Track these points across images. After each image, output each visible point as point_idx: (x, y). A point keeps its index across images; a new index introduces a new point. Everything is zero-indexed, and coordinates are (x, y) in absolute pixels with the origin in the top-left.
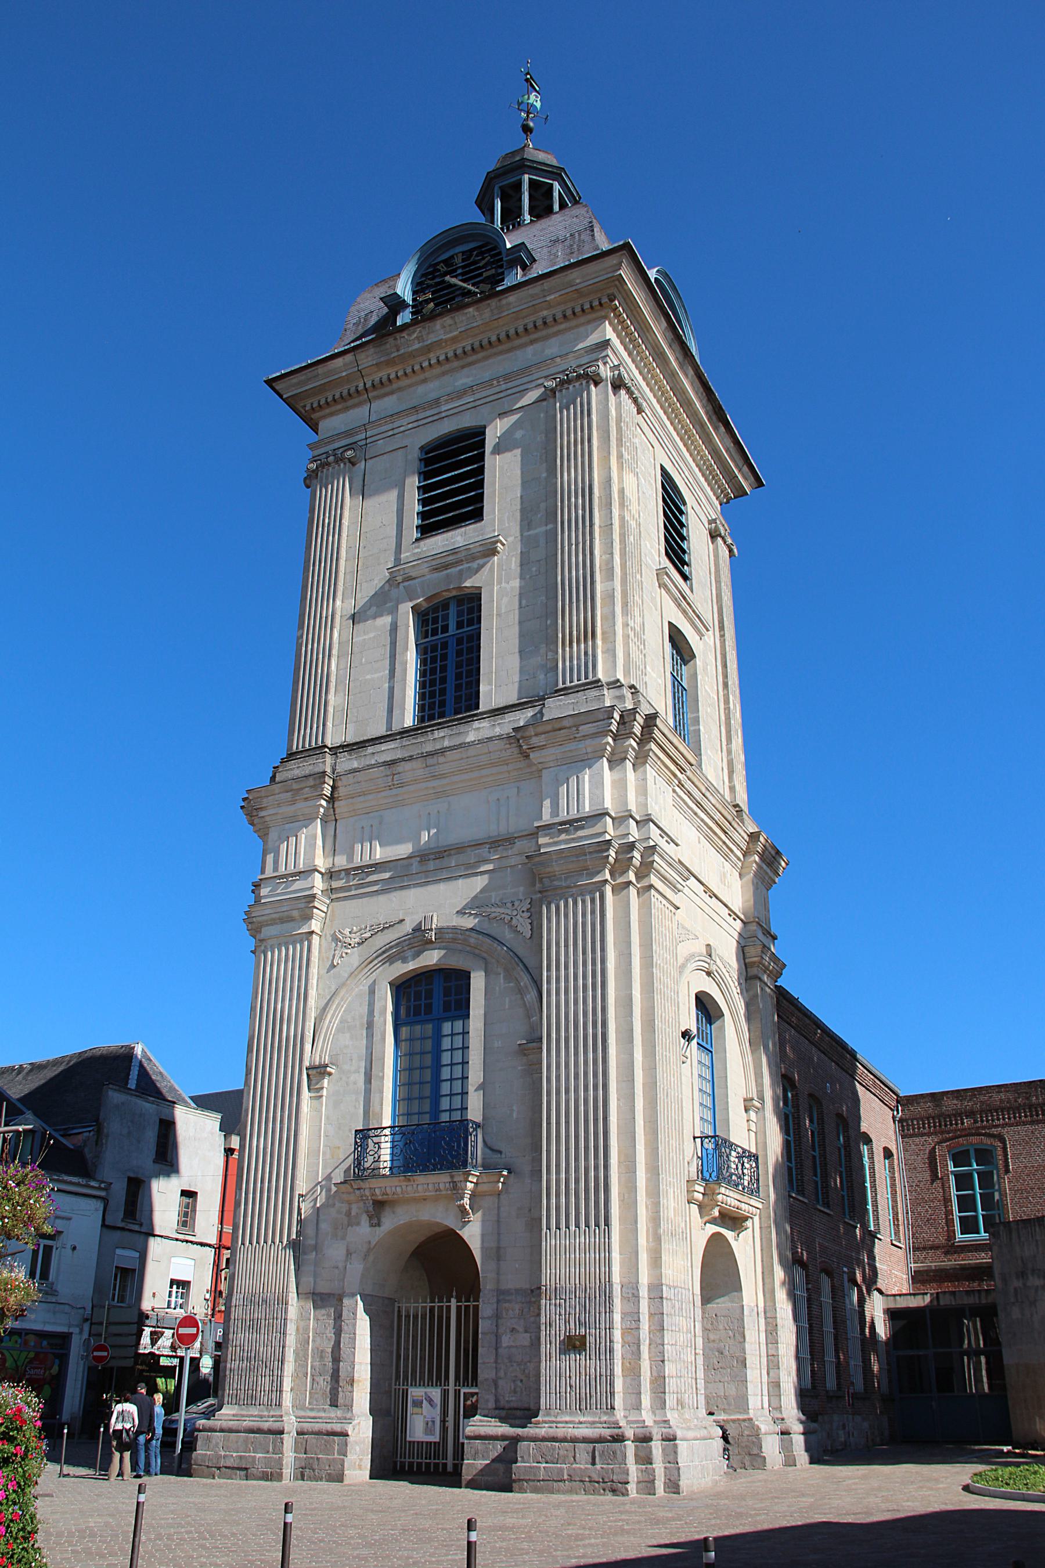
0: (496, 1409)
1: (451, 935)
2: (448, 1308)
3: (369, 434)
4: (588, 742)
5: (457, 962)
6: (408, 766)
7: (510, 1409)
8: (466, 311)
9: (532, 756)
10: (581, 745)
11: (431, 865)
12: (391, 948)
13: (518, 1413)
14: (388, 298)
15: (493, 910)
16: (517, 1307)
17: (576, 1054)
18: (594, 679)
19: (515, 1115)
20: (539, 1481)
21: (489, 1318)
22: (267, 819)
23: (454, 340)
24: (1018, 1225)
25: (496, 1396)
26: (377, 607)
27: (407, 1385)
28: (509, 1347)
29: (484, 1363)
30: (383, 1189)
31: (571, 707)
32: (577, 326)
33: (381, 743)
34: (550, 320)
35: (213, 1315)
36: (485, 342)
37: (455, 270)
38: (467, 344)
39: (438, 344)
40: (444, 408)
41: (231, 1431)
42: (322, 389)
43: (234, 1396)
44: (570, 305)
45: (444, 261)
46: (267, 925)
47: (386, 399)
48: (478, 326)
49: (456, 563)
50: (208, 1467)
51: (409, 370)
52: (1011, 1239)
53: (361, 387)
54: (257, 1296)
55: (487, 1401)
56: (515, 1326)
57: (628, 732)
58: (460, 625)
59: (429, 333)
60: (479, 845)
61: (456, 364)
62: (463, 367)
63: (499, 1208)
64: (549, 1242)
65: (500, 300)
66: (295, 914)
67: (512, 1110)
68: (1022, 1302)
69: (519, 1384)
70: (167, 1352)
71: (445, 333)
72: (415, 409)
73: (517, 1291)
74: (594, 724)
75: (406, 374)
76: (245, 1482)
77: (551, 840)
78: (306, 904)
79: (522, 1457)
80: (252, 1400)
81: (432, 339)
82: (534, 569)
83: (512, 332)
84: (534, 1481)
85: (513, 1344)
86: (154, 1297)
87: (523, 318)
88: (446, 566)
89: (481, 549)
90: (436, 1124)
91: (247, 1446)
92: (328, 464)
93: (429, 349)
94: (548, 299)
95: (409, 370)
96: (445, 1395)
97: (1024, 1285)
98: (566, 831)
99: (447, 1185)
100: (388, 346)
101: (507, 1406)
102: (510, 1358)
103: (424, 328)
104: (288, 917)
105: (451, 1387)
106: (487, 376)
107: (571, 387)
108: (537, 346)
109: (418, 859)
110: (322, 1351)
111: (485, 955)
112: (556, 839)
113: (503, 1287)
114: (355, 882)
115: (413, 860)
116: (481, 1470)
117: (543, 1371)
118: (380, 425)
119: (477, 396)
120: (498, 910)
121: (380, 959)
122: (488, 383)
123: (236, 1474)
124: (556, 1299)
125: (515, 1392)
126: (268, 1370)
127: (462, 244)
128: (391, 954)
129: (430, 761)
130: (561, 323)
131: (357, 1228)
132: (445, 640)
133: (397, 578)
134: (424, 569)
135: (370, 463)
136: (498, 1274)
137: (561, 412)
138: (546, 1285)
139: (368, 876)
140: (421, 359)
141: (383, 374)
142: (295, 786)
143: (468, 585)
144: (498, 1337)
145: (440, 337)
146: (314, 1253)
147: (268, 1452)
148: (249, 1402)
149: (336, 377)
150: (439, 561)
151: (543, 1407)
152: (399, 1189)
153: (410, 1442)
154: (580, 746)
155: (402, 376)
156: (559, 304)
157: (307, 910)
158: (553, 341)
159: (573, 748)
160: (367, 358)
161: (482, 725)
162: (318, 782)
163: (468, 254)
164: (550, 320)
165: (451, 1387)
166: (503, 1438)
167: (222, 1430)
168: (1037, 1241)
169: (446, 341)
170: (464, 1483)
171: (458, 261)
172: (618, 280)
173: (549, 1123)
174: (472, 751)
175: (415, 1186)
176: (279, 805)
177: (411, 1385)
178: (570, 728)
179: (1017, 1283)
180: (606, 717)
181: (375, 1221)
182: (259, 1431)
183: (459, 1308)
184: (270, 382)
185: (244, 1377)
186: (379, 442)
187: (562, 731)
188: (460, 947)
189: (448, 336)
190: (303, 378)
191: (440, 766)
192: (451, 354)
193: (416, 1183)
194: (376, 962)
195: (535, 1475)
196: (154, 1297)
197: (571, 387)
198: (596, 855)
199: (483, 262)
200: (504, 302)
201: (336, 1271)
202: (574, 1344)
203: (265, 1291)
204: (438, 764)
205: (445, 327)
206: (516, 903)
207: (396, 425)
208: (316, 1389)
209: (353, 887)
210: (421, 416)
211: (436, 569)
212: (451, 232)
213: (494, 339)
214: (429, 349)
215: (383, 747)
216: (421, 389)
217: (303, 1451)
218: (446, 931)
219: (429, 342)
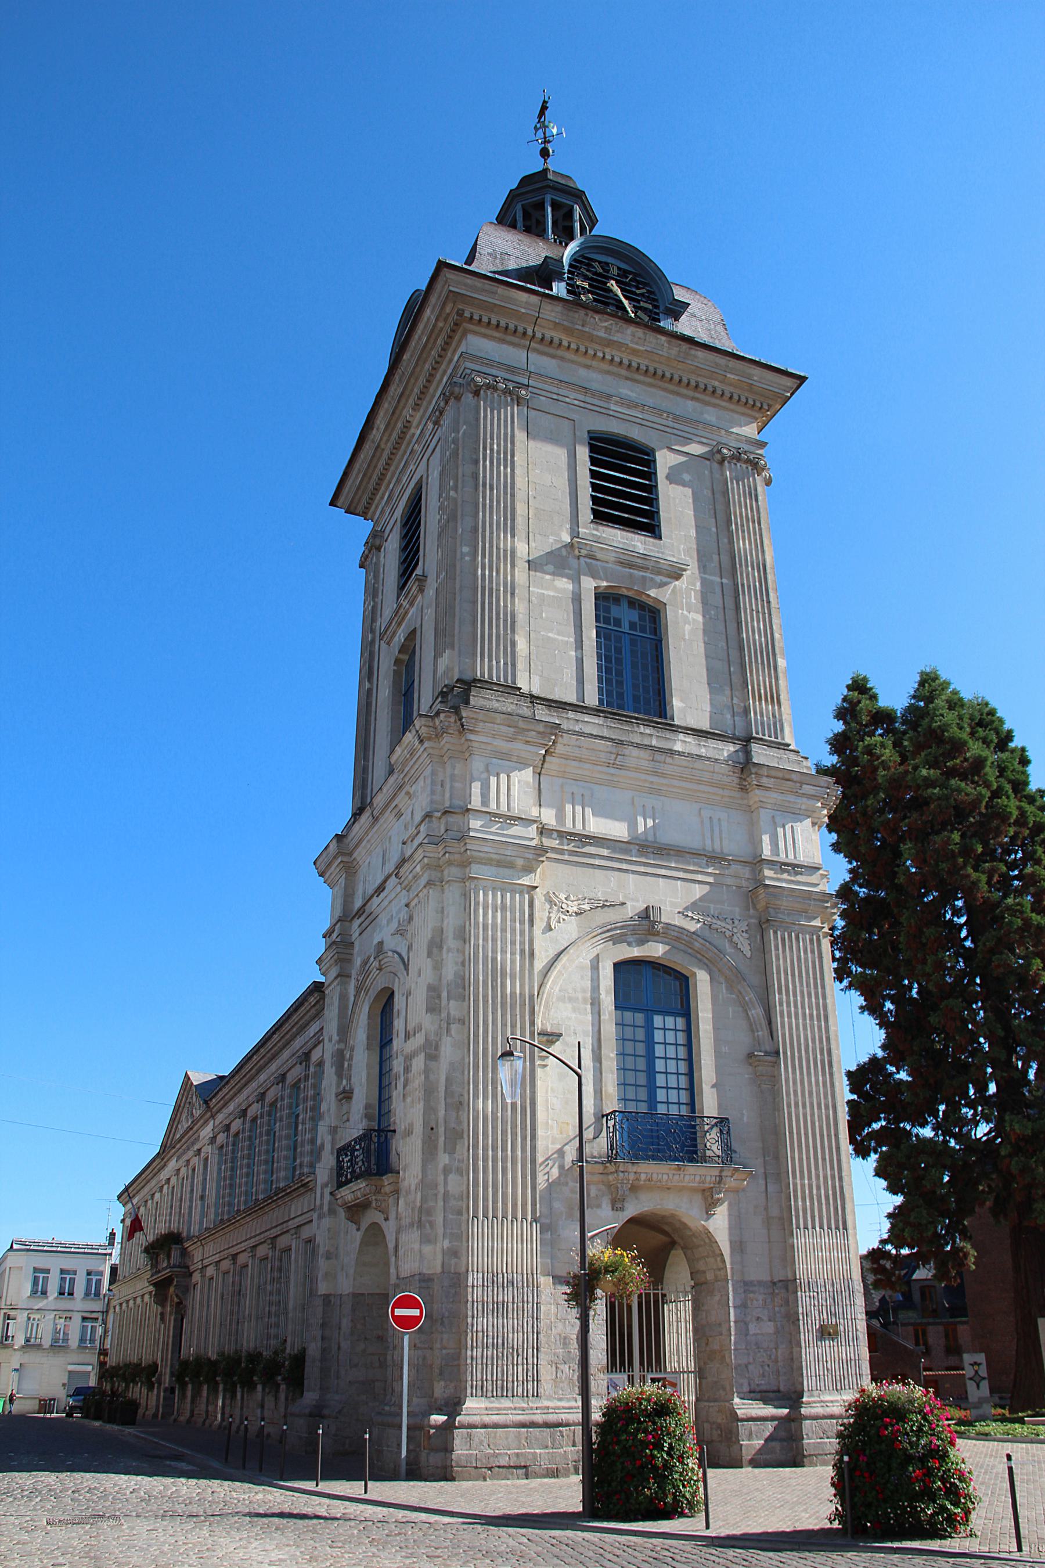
0: (750, 1392)
1: (676, 934)
5: (681, 962)
6: (635, 752)
8: (659, 336)
10: (799, 800)
12: (616, 928)
16: (761, 1298)
17: (809, 1074)
19: (745, 1119)
20: (826, 1455)
23: (635, 352)
28: (755, 1334)
30: (649, 1176)
38: (644, 363)
39: (619, 345)
40: (613, 407)
41: (496, 1426)
43: (479, 1388)
46: (479, 863)
47: (545, 358)
48: (662, 356)
49: (642, 568)
50: (476, 1467)
51: (582, 349)
53: (530, 332)
54: (500, 1276)
56: (760, 1315)
59: (618, 331)
61: (624, 372)
62: (627, 378)
64: (801, 1241)
65: (690, 348)
66: (520, 862)
67: (743, 1114)
69: (767, 1368)
71: (632, 341)
73: (760, 1283)
75: (577, 350)
76: (526, 1481)
77: (775, 876)
78: (535, 856)
79: (807, 1434)
80: (503, 1391)
81: (617, 337)
84: (822, 1455)
85: (759, 1332)
88: (631, 565)
89: (669, 568)
90: (652, 1114)
91: (520, 1442)
93: (609, 343)
98: (787, 871)
99: (714, 1178)
100: (576, 315)
101: (758, 1389)
103: (616, 324)
106: (650, 402)
107: (738, 465)
109: (637, 847)
110: (565, 1338)
112: (779, 876)
113: (747, 1278)
114: (570, 847)
115: (632, 847)
116: (760, 1449)
117: (804, 1356)
118: (545, 383)
119: (646, 417)
120: (719, 923)
121: (604, 936)
123: (513, 1473)
124: (810, 1291)
125: (764, 1376)
126: (520, 1358)
127: (615, 258)
128: (618, 935)
129: (659, 757)
130: (641, 374)
131: (599, 1211)
133: (582, 551)
134: (611, 557)
137: (732, 483)
138: (800, 1279)
139: (583, 847)
140: (597, 347)
141: (556, 335)
142: (521, 724)
143: (652, 595)
145: (626, 342)
147: (547, 1447)
148: (499, 1394)
150: (626, 557)
151: (806, 1389)
154: (798, 801)
155: (573, 349)
156: (731, 385)
157: (534, 862)
159: (792, 800)
161: (687, 740)
166: (772, 1418)
167: (485, 1426)
170: (744, 1462)
173: (791, 1133)
174: (699, 764)
175: (682, 1176)
176: (494, 736)
177: (648, 1371)
178: (795, 782)
181: (619, 1206)
182: (533, 1425)
185: (490, 1367)
188: (682, 947)
189: (635, 346)
190: (479, 285)
194: (599, 938)
195: (823, 1450)
198: (818, 903)
200: (693, 352)
203: (509, 1271)
204: (665, 763)
206: (736, 922)
208: (561, 1378)
209: (566, 852)
211: (621, 563)
212: (615, 242)
214: (609, 343)
215: (587, 718)
216: (582, 372)
217: (571, 1443)
218: (673, 928)
219: (615, 339)
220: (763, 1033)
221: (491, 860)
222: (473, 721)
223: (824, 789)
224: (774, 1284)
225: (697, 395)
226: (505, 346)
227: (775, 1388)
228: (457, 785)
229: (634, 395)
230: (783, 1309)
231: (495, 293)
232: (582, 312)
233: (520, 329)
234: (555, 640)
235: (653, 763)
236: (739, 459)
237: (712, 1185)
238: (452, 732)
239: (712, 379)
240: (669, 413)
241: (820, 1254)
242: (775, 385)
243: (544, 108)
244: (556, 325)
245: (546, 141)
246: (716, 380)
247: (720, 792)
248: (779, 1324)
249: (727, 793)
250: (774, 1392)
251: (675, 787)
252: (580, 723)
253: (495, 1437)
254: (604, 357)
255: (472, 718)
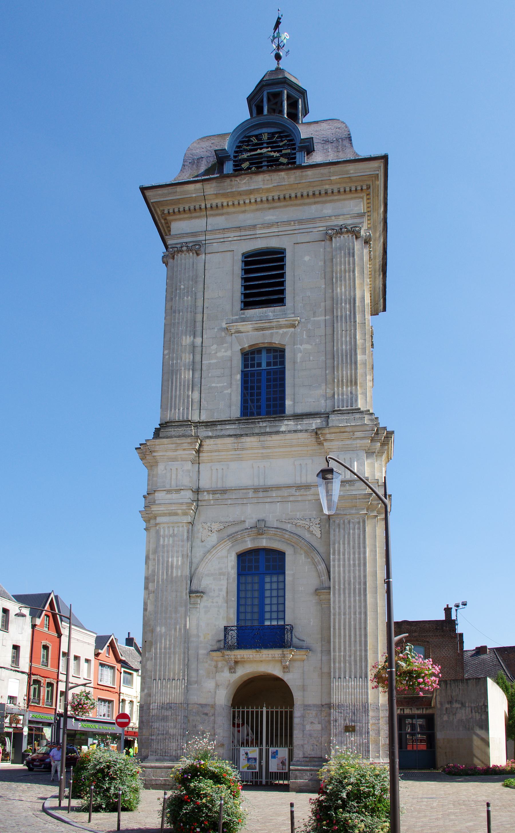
0: (304, 757)
2: (262, 712)
3: (207, 238)
4: (358, 441)
7: (310, 758)
9: (325, 444)
10: (355, 442)
11: (261, 494)
13: (316, 759)
14: (220, 152)
15: (298, 522)
18: (356, 407)
19: (312, 623)
21: (299, 717)
22: (158, 457)
23: (268, 190)
24: (451, 681)
25: (303, 752)
26: (217, 345)
27: (268, 747)
29: (297, 737)
31: (345, 421)
32: (344, 200)
33: (226, 424)
34: (330, 192)
35: (27, 708)
36: (287, 196)
37: (262, 144)
38: (276, 194)
40: (258, 232)
42: (177, 202)
44: (344, 185)
45: (256, 136)
46: (160, 516)
49: (270, 328)
51: (236, 203)
52: (446, 687)
53: (203, 206)
55: (299, 754)
57: (379, 439)
58: (268, 364)
60: (289, 487)
61: (266, 205)
62: (270, 209)
63: (303, 667)
68: (449, 714)
69: (315, 746)
70: (8, 725)
71: (264, 184)
72: (239, 228)
73: (314, 705)
74: (363, 432)
75: (233, 204)
82: (317, 340)
83: (305, 194)
86: (2, 698)
87: (313, 187)
89: (286, 323)
92: (182, 251)
94: (332, 178)
95: (236, 203)
96: (261, 751)
97: (451, 706)
99: (280, 655)
100: (226, 184)
102: (310, 735)
104: (175, 513)
105: (264, 747)
106: (285, 218)
107: (342, 237)
108: (319, 206)
109: (253, 490)
111: (293, 544)
113: (306, 703)
115: (249, 491)
118: (215, 234)
119: (281, 229)
120: (301, 522)
122: (288, 223)
125: (313, 750)
130: (336, 195)
132: (259, 371)
133: (232, 330)
135: (208, 256)
136: (304, 697)
140: (244, 197)
141: (219, 201)
144: (304, 726)
145: (260, 187)
146: (196, 685)
149: (189, 196)
152: (251, 656)
153: (270, 772)
156: (337, 183)
158: (328, 205)
160: (210, 189)
162: (193, 441)
163: (273, 134)
164: (330, 192)
165: (264, 747)
168: (459, 689)
169: (263, 190)
171: (265, 137)
172: (375, 177)
175: (261, 655)
176: (166, 451)
179: (448, 706)
180: (371, 429)
181: (232, 671)
183: (267, 712)
184: (143, 190)
186: (214, 244)
187: (344, 434)
188: (278, 538)
189: (266, 187)
191: (268, 442)
192: (264, 199)
193: (262, 653)
196: (2, 698)
197: (342, 237)
199: (281, 144)
200: (304, 174)
201: (210, 694)
202: (349, 729)
204: (267, 441)
205: (264, 180)
206: (312, 520)
207: (226, 235)
210: (243, 233)
213: (293, 195)
214: (251, 192)
216: (241, 216)
220: (325, 578)
221: (165, 513)
222: (153, 446)
223: (370, 432)
224: (323, 705)
225: (317, 200)
226: (193, 221)
227: (320, 756)
228: (155, 479)
229: (275, 217)
230: (326, 718)
231: (176, 192)
232: (228, 180)
233: (197, 207)
234: (217, 387)
235: (260, 442)
236: (341, 233)
237: (280, 659)
238: (148, 453)
239: (323, 185)
240: (294, 221)
241: (347, 690)
242: (367, 170)
243: (278, 23)
244: (217, 195)
245: (278, 47)
246: (325, 185)
247: (306, 448)
248: (323, 725)
249: (309, 448)
250: (319, 758)
251: (276, 452)
252: (223, 430)
253: (156, 772)
254: (250, 202)
255: (153, 445)
